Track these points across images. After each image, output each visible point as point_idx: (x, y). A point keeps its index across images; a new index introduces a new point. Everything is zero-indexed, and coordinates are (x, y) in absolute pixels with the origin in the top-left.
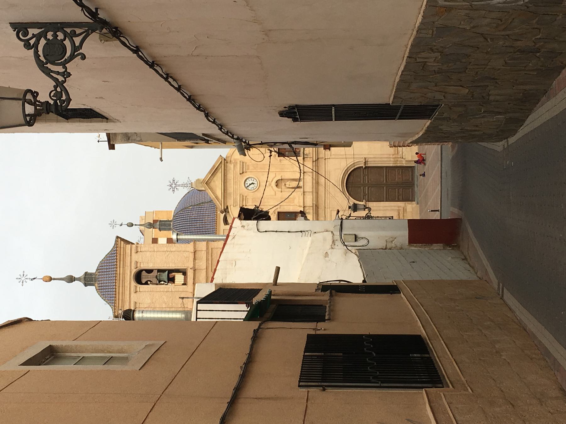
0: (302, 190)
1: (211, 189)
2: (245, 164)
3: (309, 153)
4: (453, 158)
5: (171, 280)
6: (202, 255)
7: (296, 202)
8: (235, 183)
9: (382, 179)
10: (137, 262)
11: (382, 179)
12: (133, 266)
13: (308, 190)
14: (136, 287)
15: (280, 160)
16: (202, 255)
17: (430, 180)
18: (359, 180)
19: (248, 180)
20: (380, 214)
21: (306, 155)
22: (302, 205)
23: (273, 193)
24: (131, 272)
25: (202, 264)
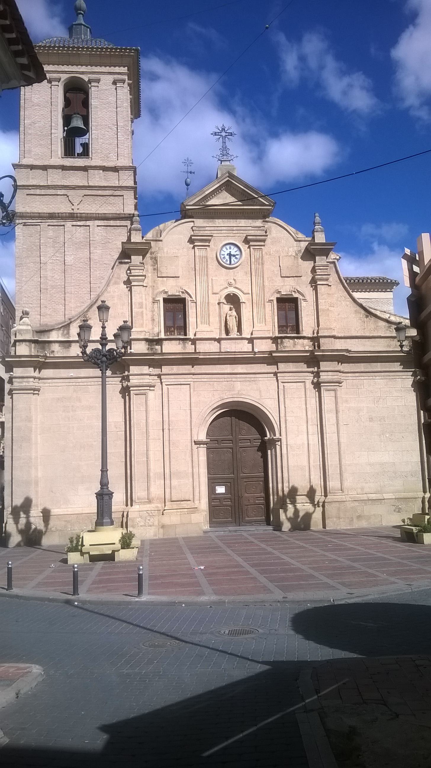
0: (224, 336)
1: (423, 508)
2: (263, 244)
3: (284, 347)
4: (292, 618)
5: (17, 54)
6: (112, 180)
7: (201, 327)
8: (231, 229)
9: (245, 471)
10: (98, 81)
11: (245, 471)
12: (93, 76)
13: (222, 347)
14: (59, 80)
15: (271, 301)
16: (112, 180)
17: (239, 559)
18: (243, 432)
19: (236, 249)
20: (137, 416)
21: (282, 342)
22: (198, 336)
23: (216, 289)
24: (83, 73)
25: (97, 179)
